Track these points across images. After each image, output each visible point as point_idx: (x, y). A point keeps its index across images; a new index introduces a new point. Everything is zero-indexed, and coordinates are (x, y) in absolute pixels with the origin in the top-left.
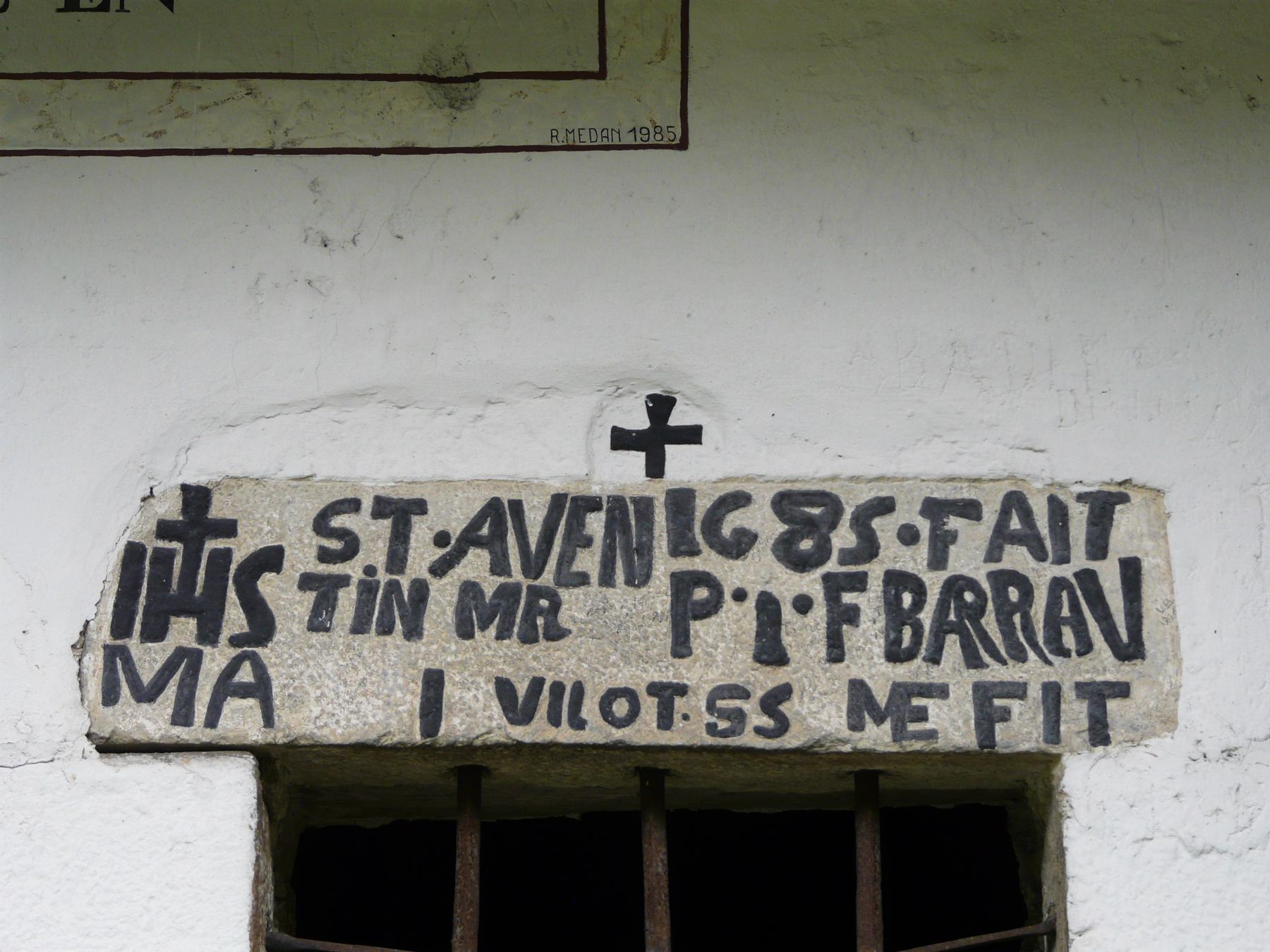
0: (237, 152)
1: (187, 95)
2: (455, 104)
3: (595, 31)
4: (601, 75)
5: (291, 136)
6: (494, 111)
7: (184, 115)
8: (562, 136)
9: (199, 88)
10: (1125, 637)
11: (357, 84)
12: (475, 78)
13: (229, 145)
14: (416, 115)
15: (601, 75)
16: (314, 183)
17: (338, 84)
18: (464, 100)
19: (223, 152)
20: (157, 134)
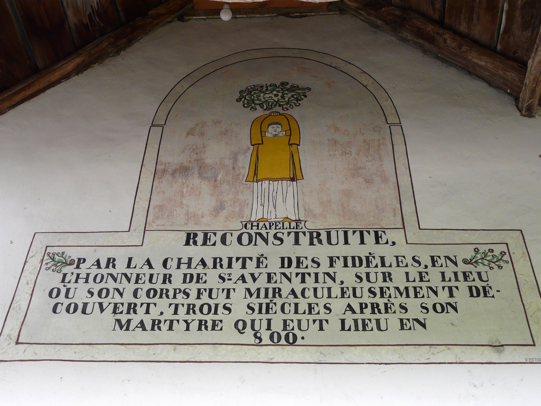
0: (448, 363)
1: (434, 349)
2: (500, 352)
3: (530, 334)
4: (262, 144)
5: (461, 359)
6: (509, 354)
7: (434, 354)
8: (528, 360)
9: (190, 239)
10: (292, 15)
11: (474, 347)
12: (502, 346)
13: (446, 362)
14: (489, 354)
15: (262, 144)
16: (469, 371)
17: (469, 347)
18: (501, 351)
19: (445, 363)
20: (428, 359)
